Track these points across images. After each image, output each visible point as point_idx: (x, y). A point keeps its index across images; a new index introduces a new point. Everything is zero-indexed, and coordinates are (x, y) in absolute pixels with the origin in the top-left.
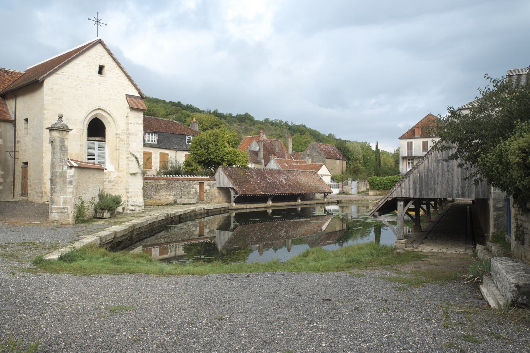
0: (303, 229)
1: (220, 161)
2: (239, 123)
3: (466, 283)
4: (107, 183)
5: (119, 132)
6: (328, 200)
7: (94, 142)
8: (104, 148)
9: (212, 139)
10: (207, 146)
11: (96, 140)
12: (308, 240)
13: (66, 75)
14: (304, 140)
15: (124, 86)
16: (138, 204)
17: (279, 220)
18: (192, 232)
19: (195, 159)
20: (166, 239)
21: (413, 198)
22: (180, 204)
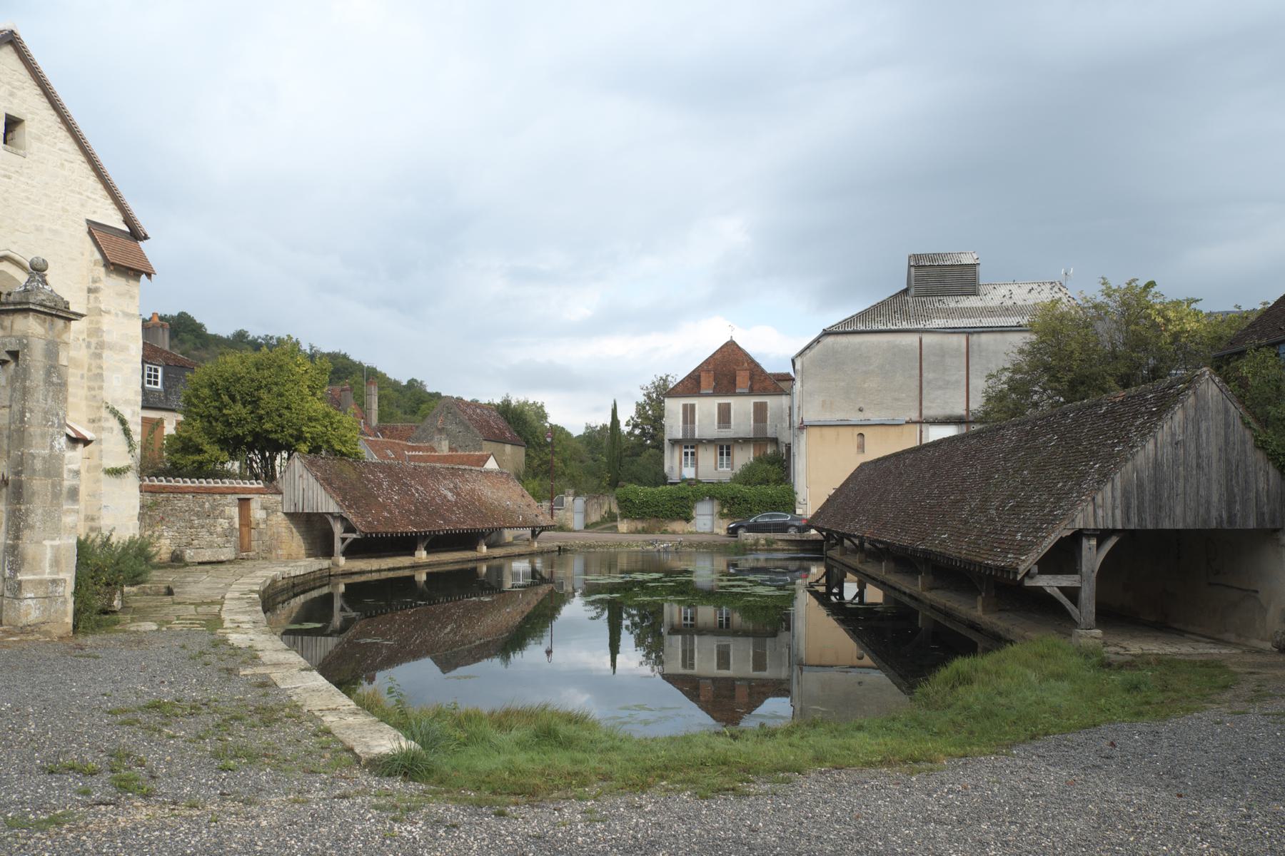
15: (79, 193)
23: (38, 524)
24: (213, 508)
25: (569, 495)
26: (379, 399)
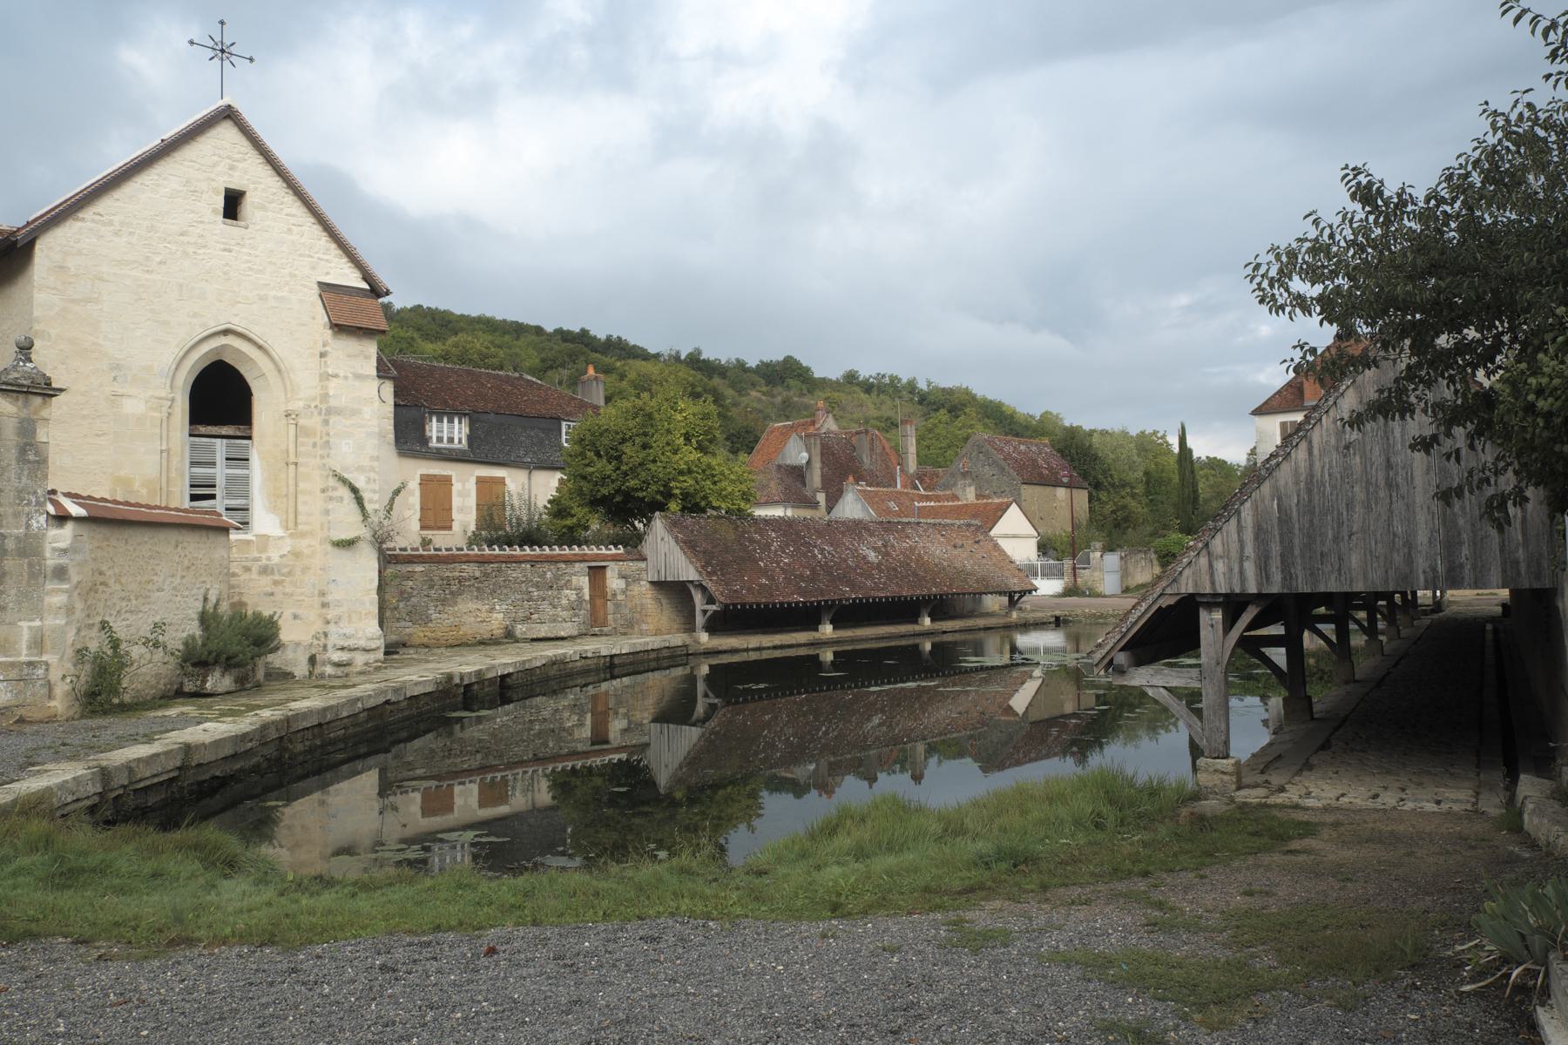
0: (942, 714)
1: (659, 497)
2: (764, 389)
3: (1468, 993)
4: (254, 575)
5: (297, 405)
6: (1022, 615)
7: (213, 440)
8: (247, 460)
9: (631, 425)
10: (617, 450)
11: (224, 433)
12: (972, 745)
13: (111, 223)
14: (959, 432)
15: (310, 256)
16: (362, 643)
17: (856, 687)
18: (570, 731)
19: (580, 492)
20: (479, 756)
21: (1259, 596)
22: (525, 640)
23: (11, 605)
24: (557, 578)
25: (1096, 550)
26: (917, 440)
